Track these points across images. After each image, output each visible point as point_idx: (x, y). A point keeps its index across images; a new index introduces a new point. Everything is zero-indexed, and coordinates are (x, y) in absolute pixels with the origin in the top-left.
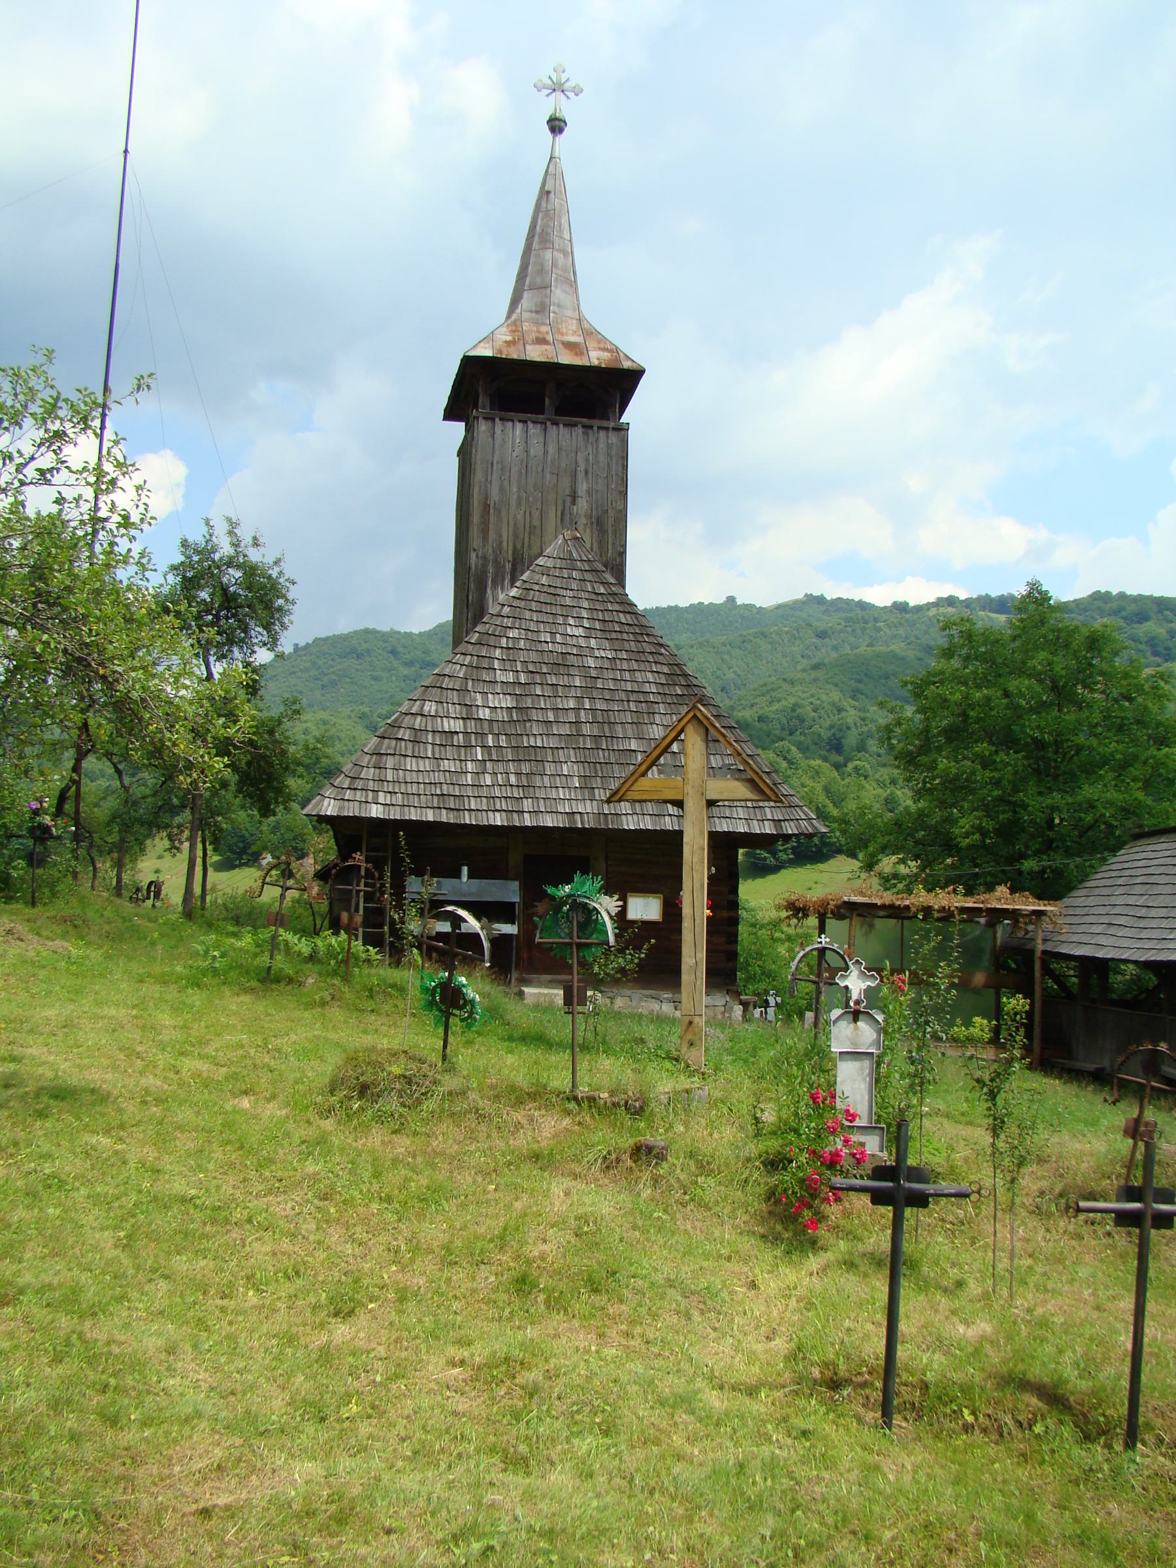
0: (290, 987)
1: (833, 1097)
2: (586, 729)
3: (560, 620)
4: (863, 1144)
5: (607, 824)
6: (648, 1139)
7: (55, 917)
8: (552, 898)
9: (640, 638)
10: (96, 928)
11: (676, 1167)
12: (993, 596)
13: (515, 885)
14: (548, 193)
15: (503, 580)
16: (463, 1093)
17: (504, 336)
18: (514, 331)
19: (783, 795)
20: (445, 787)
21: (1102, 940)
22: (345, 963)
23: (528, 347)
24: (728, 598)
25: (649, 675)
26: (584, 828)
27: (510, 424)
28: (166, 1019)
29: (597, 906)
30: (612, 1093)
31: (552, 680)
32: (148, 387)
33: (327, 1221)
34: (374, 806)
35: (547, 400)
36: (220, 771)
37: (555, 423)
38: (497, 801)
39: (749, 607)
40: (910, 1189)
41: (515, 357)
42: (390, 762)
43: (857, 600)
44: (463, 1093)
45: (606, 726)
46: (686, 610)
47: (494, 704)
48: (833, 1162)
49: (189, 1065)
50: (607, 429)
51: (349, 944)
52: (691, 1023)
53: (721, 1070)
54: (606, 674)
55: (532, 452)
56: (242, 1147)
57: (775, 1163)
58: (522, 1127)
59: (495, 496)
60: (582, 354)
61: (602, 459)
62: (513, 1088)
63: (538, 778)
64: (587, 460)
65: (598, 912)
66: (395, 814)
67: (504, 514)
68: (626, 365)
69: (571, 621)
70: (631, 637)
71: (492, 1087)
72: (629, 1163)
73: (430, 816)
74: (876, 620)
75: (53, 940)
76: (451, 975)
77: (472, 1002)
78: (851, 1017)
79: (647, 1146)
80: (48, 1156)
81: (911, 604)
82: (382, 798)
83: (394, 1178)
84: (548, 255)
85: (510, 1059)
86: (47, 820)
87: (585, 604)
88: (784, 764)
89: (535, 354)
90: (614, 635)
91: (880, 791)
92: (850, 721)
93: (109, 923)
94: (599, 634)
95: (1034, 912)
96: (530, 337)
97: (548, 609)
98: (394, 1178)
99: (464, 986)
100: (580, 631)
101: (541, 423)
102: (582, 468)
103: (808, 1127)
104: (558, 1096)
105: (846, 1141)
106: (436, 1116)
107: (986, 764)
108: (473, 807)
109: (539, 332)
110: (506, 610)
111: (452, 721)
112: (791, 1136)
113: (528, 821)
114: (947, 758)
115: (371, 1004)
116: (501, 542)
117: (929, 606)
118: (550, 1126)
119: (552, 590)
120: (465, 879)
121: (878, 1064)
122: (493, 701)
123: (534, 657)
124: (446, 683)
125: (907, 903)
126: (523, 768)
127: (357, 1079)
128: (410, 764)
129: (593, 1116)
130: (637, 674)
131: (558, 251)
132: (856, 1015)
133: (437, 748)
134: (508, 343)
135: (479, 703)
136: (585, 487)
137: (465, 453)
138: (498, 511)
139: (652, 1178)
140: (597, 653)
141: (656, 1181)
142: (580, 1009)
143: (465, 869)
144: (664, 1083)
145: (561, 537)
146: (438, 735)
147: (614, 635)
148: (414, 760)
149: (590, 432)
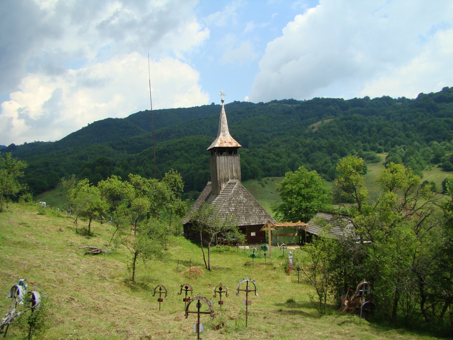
11: (277, 269)
21: (315, 231)
57: (285, 268)
81: (264, 103)
91: (260, 160)
92: (250, 139)
96: (223, 141)
107: (296, 199)
117: (269, 103)
128: (223, 218)
134: (221, 143)
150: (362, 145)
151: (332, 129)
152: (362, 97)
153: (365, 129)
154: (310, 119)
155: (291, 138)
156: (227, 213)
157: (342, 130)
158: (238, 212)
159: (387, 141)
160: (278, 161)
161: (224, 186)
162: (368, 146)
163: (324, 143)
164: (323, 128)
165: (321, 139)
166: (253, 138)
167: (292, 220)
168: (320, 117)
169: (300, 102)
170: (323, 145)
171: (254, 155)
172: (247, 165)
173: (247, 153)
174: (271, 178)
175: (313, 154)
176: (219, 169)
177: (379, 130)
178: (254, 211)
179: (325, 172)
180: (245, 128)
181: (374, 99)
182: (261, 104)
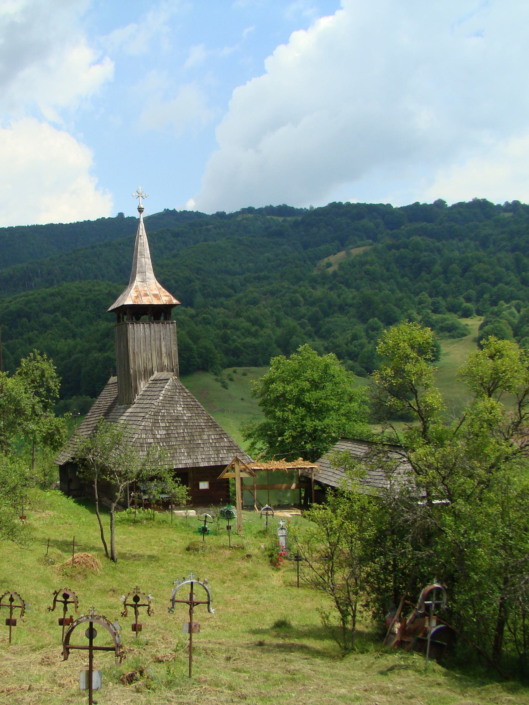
2: (187, 438)
11: (254, 558)
12: (274, 206)
24: (119, 214)
31: (175, 424)
41: (139, 303)
55: (146, 334)
57: (271, 556)
67: (140, 355)
84: (143, 260)
87: (181, 400)
92: (197, 287)
95: (310, 468)
96: (142, 293)
97: (171, 402)
100: (181, 409)
102: (162, 337)
107: (293, 412)
109: (144, 291)
115: (161, 526)
117: (237, 214)
123: (169, 418)
124: (147, 428)
138: (138, 355)
141: (252, 561)
144: (245, 542)
150: (430, 300)
151: (368, 267)
152: (430, 201)
153: (437, 268)
154: (322, 248)
155: (283, 287)
157: (388, 270)
158: (174, 440)
159: (481, 294)
160: (255, 335)
162: (443, 303)
163: (351, 296)
164: (349, 264)
165: (344, 287)
166: (204, 286)
168: (343, 243)
169: (300, 212)
170: (349, 301)
172: (190, 342)
173: (192, 317)
174: (240, 370)
175: (327, 319)
176: (134, 350)
177: (465, 270)
178: (205, 437)
179: (353, 356)
180: (187, 266)
181: (454, 206)
182: (220, 215)
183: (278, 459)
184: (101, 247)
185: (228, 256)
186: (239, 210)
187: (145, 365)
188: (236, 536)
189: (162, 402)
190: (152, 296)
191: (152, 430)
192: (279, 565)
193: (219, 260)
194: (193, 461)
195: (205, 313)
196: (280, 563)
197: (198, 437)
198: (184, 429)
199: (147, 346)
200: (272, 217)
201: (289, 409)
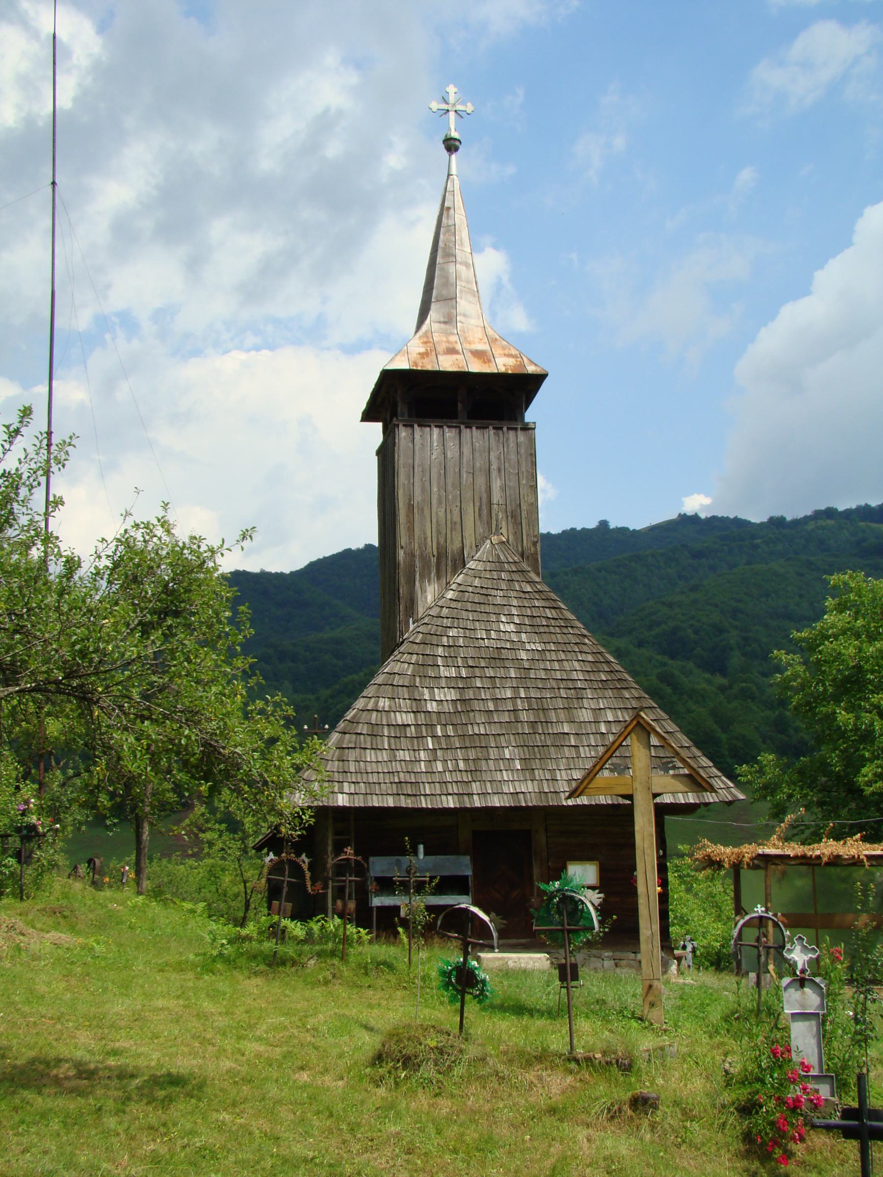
0: (293, 969)
1: (789, 1051)
2: (524, 716)
3: (493, 618)
4: (817, 1091)
5: (548, 801)
6: (640, 1090)
7: (44, 909)
8: (544, 893)
9: (565, 631)
10: (83, 917)
11: (667, 1115)
13: (466, 860)
14: (449, 209)
15: (430, 573)
16: (483, 1059)
17: (416, 347)
18: (425, 343)
19: (703, 767)
20: (402, 775)
22: (341, 948)
23: (440, 358)
25: (576, 664)
26: (527, 807)
27: (428, 429)
28: (208, 1006)
29: (583, 898)
30: (604, 1053)
31: (490, 672)
32: (251, 536)
33: (416, 1171)
34: (340, 796)
35: (460, 406)
36: (307, 821)
37: (469, 427)
38: (449, 785)
39: (623, 530)
40: (871, 1125)
41: (429, 368)
42: (352, 755)
43: (732, 517)
44: (483, 1059)
45: (541, 712)
46: (558, 536)
47: (439, 698)
48: (795, 1106)
49: (251, 1047)
50: (516, 429)
51: (345, 928)
52: (650, 986)
53: (680, 1027)
54: (537, 665)
55: (449, 455)
56: (331, 1115)
57: (747, 1109)
58: (536, 1086)
59: (418, 498)
60: (489, 361)
61: (513, 457)
62: (521, 1053)
63: (483, 762)
64: (499, 459)
65: (583, 903)
66: (359, 802)
67: (427, 512)
68: (531, 369)
69: (503, 619)
70: (558, 630)
71: (505, 1053)
72: (629, 1112)
73: (390, 802)
74: (753, 537)
75: (48, 932)
76: (465, 959)
77: (483, 982)
78: (798, 984)
79: (643, 1098)
80: (192, 1133)
82: (346, 788)
83: (452, 1131)
84: (451, 268)
85: (504, 1025)
86: (33, 819)
87: (515, 602)
88: (669, 690)
89: (447, 364)
90: (542, 629)
92: (732, 642)
93: (91, 911)
94: (529, 629)
96: (441, 348)
97: (482, 608)
98: (452, 1131)
99: (476, 968)
100: (511, 628)
101: (456, 427)
102: (494, 466)
103: (771, 1077)
104: (560, 1058)
105: (805, 1089)
106: (467, 1079)
108: (428, 792)
109: (448, 342)
110: (445, 612)
111: (404, 715)
112: (758, 1086)
113: (477, 803)
114: (845, 710)
115: (366, 981)
116: (425, 539)
118: (556, 1084)
119: (484, 591)
120: (421, 856)
121: (824, 1022)
122: (439, 695)
123: (471, 652)
124: (397, 680)
125: (818, 853)
126: (470, 754)
127: (400, 1052)
128: (370, 756)
129: (591, 1074)
130: (565, 663)
131: (461, 263)
132: (802, 983)
133: (392, 740)
134: (423, 355)
135: (427, 697)
136: (499, 484)
137: (386, 455)
139: (650, 1125)
140: (528, 647)
141: (653, 1127)
142: (574, 983)
143: (421, 848)
144: (646, 1042)
145: (488, 541)
146: (392, 728)
147: (542, 629)
148: (373, 751)
149: (500, 432)
156: (400, 719)
158: (480, 718)
161: (429, 594)
166: (746, 639)
167: (860, 828)
171: (746, 695)
172: (715, 727)
173: (722, 689)
176: (411, 498)
178: (585, 715)
180: (716, 606)
182: (777, 523)
183: (839, 836)
184: (566, 574)
185: (789, 589)
186: (809, 513)
187: (442, 541)
188: (634, 1024)
189: (454, 605)
190: (469, 355)
191: (412, 687)
192: (788, 1155)
193: (773, 595)
194: (540, 786)
195: (745, 681)
196: (792, 1146)
197: (562, 715)
198: (515, 689)
199: (450, 488)
200: (869, 524)
201: (872, 705)
